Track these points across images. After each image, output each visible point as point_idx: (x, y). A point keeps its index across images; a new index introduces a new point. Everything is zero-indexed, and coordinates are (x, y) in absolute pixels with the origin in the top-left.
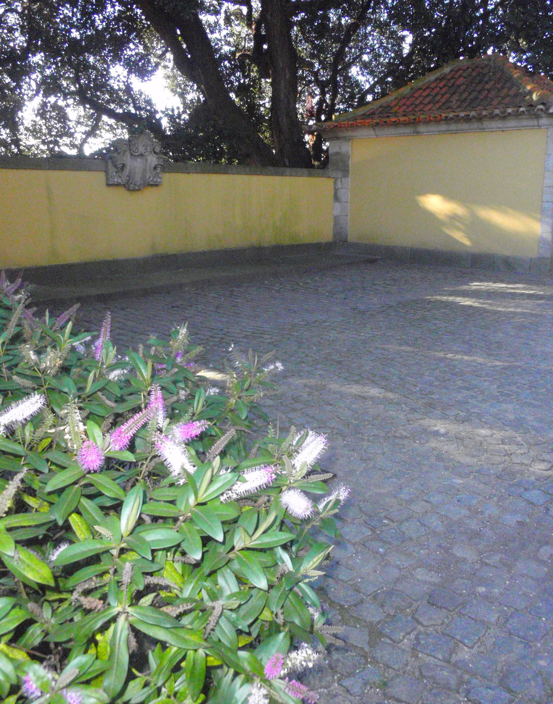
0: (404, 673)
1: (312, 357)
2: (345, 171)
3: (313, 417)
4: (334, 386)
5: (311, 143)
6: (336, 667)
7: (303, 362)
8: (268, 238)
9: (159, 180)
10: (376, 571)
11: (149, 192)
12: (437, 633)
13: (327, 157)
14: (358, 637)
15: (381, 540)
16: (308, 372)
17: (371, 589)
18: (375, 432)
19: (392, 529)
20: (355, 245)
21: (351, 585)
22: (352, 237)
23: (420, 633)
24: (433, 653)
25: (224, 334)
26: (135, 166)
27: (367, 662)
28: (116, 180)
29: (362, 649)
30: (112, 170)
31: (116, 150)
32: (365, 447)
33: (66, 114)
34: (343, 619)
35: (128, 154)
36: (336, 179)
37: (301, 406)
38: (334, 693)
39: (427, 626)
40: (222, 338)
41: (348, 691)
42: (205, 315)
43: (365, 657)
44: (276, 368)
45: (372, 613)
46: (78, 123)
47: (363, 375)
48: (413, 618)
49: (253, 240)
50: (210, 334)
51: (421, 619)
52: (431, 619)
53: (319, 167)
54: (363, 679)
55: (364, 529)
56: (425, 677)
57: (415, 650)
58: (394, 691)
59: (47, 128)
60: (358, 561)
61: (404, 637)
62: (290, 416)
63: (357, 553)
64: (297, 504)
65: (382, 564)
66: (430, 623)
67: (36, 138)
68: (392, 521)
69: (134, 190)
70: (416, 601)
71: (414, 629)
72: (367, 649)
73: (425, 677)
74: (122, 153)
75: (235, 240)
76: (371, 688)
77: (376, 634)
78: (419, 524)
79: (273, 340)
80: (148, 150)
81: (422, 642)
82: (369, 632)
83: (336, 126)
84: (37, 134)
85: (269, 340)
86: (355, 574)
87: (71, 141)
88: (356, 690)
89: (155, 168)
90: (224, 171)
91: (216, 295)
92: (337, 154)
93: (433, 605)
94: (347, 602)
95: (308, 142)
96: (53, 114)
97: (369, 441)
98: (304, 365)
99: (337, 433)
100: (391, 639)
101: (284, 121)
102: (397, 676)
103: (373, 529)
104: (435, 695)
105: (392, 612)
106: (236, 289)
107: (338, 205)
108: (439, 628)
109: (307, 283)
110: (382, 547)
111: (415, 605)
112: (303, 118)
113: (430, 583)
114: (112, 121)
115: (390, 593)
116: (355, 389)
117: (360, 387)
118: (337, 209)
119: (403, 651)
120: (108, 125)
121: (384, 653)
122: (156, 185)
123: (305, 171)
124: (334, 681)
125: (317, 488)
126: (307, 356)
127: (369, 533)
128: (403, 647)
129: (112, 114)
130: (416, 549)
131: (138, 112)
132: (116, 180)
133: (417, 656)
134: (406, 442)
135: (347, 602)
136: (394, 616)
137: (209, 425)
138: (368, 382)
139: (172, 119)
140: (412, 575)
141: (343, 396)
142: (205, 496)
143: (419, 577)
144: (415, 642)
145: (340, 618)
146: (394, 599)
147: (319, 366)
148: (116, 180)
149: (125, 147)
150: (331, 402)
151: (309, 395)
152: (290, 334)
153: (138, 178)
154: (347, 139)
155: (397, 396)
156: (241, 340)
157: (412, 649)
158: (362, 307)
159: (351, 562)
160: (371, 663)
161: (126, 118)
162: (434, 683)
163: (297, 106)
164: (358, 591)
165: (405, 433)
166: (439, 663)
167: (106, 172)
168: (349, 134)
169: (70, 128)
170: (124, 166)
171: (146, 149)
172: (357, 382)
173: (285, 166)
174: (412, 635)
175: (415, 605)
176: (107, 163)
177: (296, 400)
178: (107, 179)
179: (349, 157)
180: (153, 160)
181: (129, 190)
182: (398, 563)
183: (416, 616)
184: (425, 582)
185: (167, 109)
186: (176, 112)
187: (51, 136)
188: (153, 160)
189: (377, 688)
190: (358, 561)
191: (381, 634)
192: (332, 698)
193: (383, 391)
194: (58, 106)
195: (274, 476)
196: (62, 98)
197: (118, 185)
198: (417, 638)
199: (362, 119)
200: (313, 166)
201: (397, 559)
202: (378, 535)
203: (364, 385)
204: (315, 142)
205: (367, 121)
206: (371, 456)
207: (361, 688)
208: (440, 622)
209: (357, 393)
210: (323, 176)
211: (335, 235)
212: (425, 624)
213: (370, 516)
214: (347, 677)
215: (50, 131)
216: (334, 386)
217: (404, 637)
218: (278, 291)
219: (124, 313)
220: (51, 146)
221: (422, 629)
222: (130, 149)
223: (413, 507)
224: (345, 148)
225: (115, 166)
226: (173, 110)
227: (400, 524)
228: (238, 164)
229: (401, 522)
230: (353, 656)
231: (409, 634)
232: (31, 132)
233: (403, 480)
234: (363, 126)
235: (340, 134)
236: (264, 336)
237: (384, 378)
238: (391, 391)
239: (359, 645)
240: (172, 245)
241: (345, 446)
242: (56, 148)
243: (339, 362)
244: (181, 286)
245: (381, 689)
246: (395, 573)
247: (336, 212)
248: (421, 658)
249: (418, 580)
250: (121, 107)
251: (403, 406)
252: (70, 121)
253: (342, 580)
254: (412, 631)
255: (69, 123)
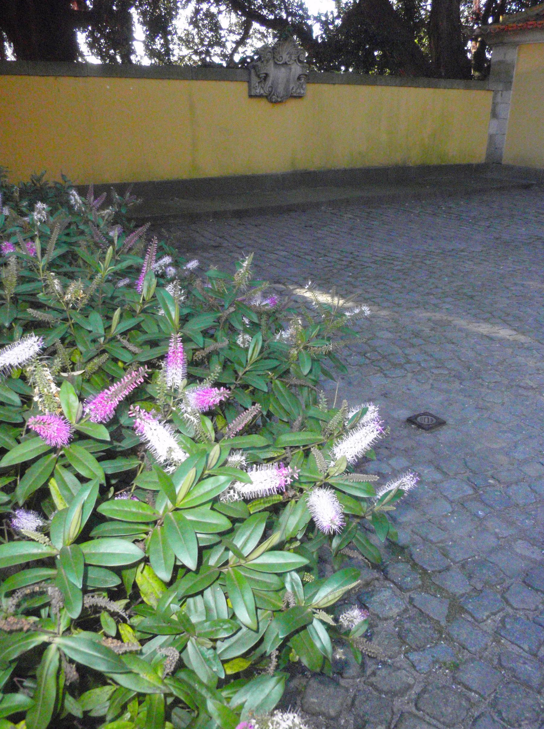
0: (480, 658)
1: (441, 288)
2: (508, 83)
3: (431, 356)
4: (462, 323)
5: (473, 51)
6: (405, 637)
7: (432, 294)
8: (415, 158)
9: (302, 91)
10: (470, 537)
11: (292, 105)
12: (528, 618)
13: (489, 66)
14: (437, 608)
15: (482, 502)
16: (434, 305)
17: (460, 557)
18: (498, 378)
19: (497, 491)
20: (509, 168)
21: (440, 548)
22: (507, 158)
23: (508, 615)
24: (518, 642)
25: (353, 258)
26: (278, 75)
27: (440, 639)
28: (258, 91)
29: (438, 622)
30: (255, 80)
31: (259, 59)
32: (483, 395)
33: (218, 21)
34: (423, 584)
35: (271, 62)
36: (496, 92)
37: (421, 341)
38: (398, 665)
39: (516, 609)
40: (351, 262)
41: (414, 666)
42: (337, 236)
43: (440, 633)
44: (362, 312)
45: (456, 583)
46: (231, 31)
47: (495, 313)
48: (503, 597)
49: (396, 158)
50: (339, 256)
51: (512, 600)
52: (523, 601)
53: (479, 79)
54: (433, 657)
55: (466, 487)
56: (504, 668)
57: (497, 635)
58: (464, 677)
59: (199, 38)
60: (452, 521)
61: (488, 617)
62: (407, 352)
63: (452, 512)
64: (326, 509)
65: (479, 529)
66: (522, 606)
67: (189, 48)
68: (499, 482)
69: (276, 102)
70: (510, 578)
71: (503, 609)
72: (443, 623)
73: (504, 668)
74: (265, 62)
75: (379, 158)
76: (440, 668)
77: (456, 608)
78: (529, 489)
79: (403, 268)
80: (293, 58)
81: (508, 626)
82: (450, 604)
83: (503, 29)
84: (189, 44)
85: (399, 267)
86: (446, 536)
87: (222, 51)
88: (423, 667)
89: (299, 78)
90: (373, 82)
91: (350, 216)
92: (500, 62)
93: (529, 586)
94: (432, 566)
95: (470, 51)
96: (206, 22)
97: (488, 388)
98: (432, 297)
99: (454, 376)
100: (473, 617)
101: (444, 25)
102: (472, 660)
103: (475, 488)
104: (512, 691)
105: (479, 586)
106: (374, 210)
107: (495, 122)
108: (531, 615)
109: (450, 208)
110: (482, 510)
111: (508, 581)
112: (467, 21)
113: (529, 559)
114: (263, 29)
115: (482, 563)
116: (484, 329)
117: (490, 326)
118: (493, 127)
119: (485, 633)
120: (260, 33)
121: (462, 632)
122: (300, 97)
123: (463, 82)
124: (399, 653)
125: (359, 489)
126: (437, 287)
127: (471, 492)
128: (485, 628)
129: (263, 21)
130: (521, 518)
131: (289, 19)
132: (259, 91)
133: (500, 641)
134: (531, 393)
135: (432, 566)
136: (481, 591)
137: (228, 394)
138: (499, 321)
139: (325, 24)
140: (510, 546)
141: (468, 334)
142: (186, 500)
143: (518, 551)
144: (500, 625)
145: (420, 583)
146: (484, 571)
147: (447, 300)
148: (258, 91)
149: (269, 56)
150: (454, 341)
151: (431, 330)
152: (422, 262)
153: (281, 89)
154: (516, 45)
155: (529, 340)
156: (370, 264)
157: (495, 632)
158: (506, 237)
159: (444, 522)
160: (446, 639)
161: (277, 24)
162: (514, 676)
163: (462, 8)
164: (445, 554)
165: (531, 383)
166: (524, 654)
167: (249, 82)
168: (517, 39)
169: (221, 37)
170: (267, 75)
171: (290, 57)
172: (486, 320)
173: (440, 77)
174: (497, 616)
175: (508, 581)
176: (250, 74)
177: (417, 334)
178: (250, 90)
179: (514, 67)
180: (297, 69)
181: (271, 102)
182: (497, 530)
183: (506, 596)
184: (524, 557)
185: (320, 15)
186: (330, 17)
187: (203, 45)
188: (297, 69)
189: (447, 669)
190: (452, 521)
191: (462, 610)
192: (394, 671)
193: (514, 333)
194: (210, 12)
195: (289, 480)
196: (215, 5)
197: (260, 96)
198: (503, 621)
199: (535, 20)
200: (471, 77)
201: (495, 526)
202: (480, 495)
203: (493, 324)
204: (478, 49)
205: (539, 22)
206: (489, 405)
207: (429, 666)
208: (534, 607)
209: (485, 333)
210: (482, 88)
211: (488, 156)
212: (515, 606)
213: (475, 473)
214: (416, 650)
215: (202, 40)
216: (462, 323)
217: (488, 617)
218: (418, 215)
219: (257, 229)
220: (203, 56)
221: (510, 611)
222: (274, 58)
223: (525, 469)
224: (510, 55)
225: (258, 76)
226: (326, 15)
227: (508, 486)
228: (390, 74)
229: (508, 485)
230: (426, 628)
231: (495, 614)
232: (184, 42)
233: (519, 437)
234: (534, 29)
235: (506, 39)
236: (395, 263)
237: (518, 318)
238: (523, 333)
239: (436, 618)
240: (313, 160)
241: (462, 391)
242: (208, 59)
243: (472, 297)
244: (318, 205)
245: (451, 672)
246: (492, 542)
247: (492, 131)
248: (503, 645)
249: (517, 554)
250: (272, 12)
251: (535, 352)
252: (221, 29)
253: (431, 542)
254: (499, 612)
255: (220, 32)
